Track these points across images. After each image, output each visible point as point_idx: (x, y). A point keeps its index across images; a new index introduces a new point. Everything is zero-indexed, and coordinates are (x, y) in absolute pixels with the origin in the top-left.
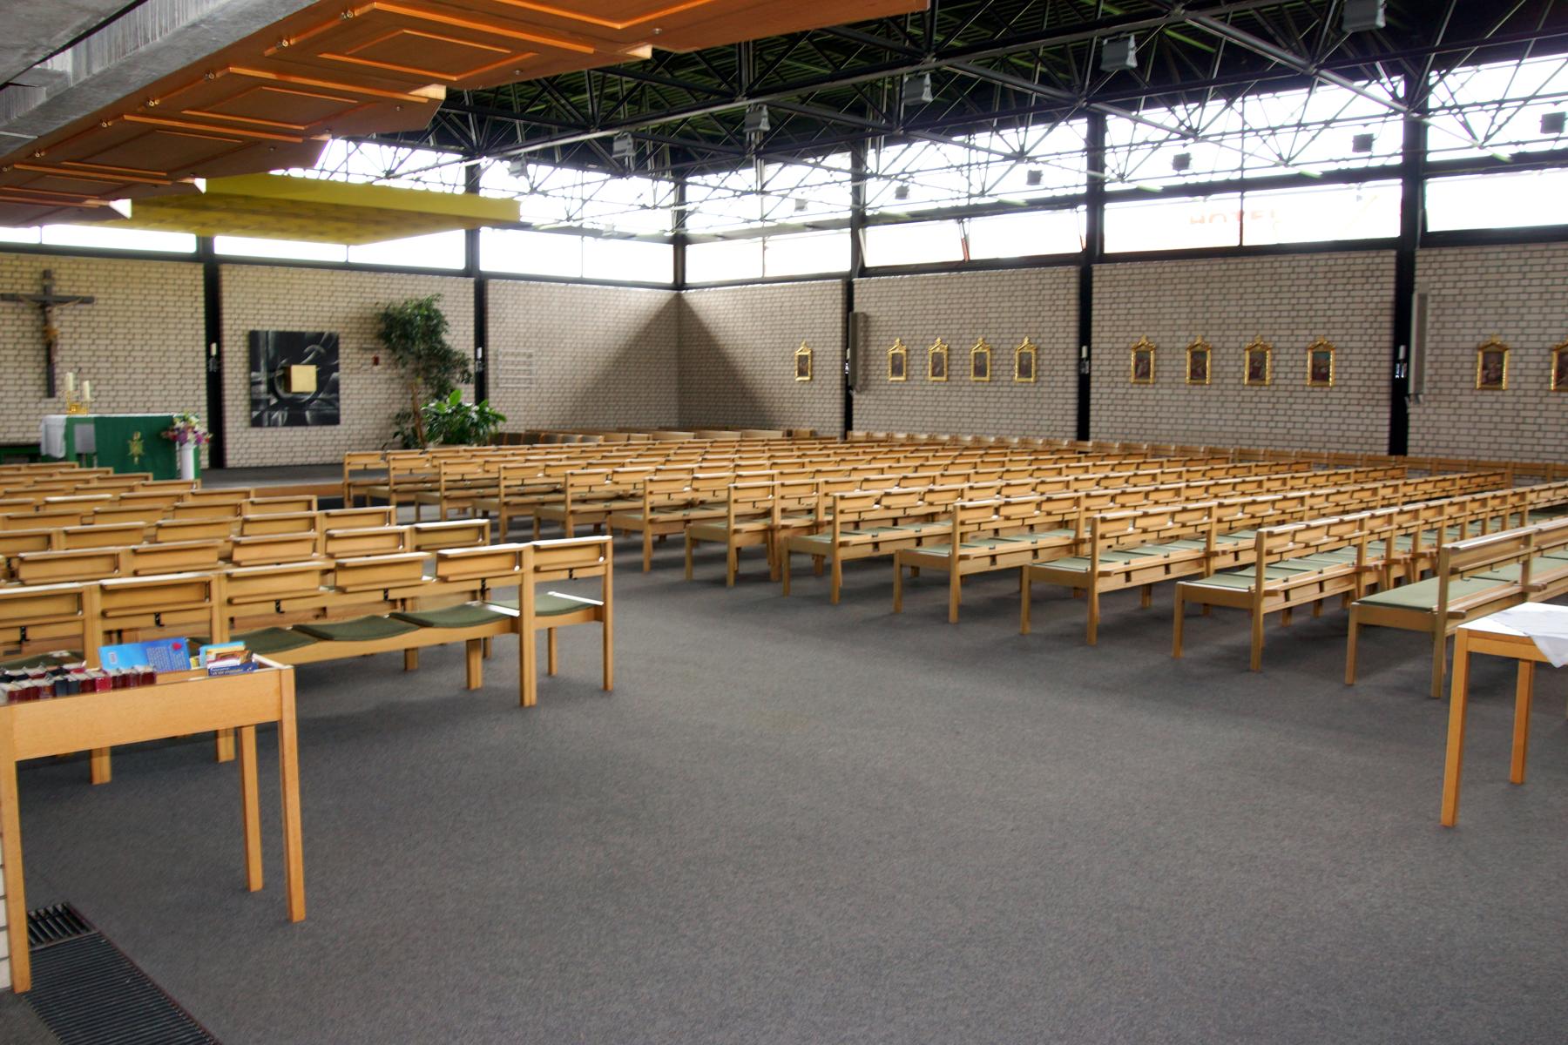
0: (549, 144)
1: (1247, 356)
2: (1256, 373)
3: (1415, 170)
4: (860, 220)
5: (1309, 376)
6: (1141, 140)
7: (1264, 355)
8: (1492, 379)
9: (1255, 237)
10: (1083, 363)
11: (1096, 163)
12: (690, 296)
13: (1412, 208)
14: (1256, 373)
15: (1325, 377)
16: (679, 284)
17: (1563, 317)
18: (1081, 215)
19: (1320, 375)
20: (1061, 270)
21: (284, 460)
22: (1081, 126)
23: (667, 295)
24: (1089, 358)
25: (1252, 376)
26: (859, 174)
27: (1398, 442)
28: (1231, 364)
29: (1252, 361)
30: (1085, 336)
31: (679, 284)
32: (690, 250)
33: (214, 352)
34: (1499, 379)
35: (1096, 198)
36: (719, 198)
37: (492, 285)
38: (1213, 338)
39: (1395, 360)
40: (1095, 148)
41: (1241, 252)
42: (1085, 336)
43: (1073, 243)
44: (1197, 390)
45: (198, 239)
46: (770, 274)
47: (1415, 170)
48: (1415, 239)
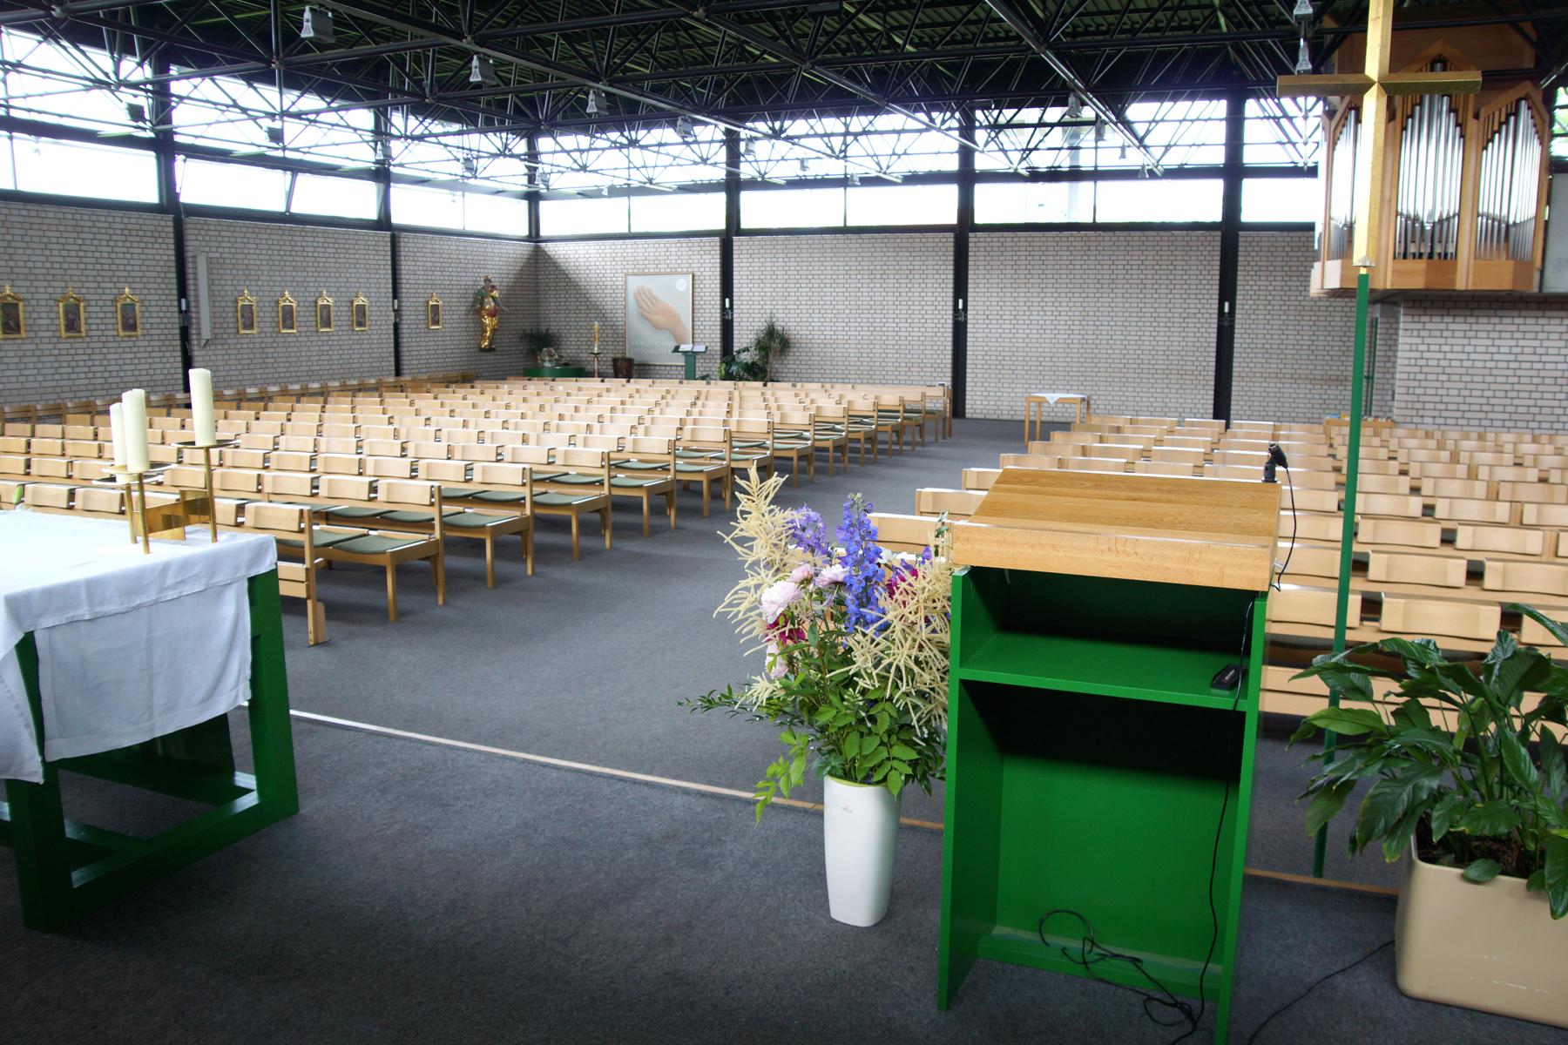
0: (636, 97)
2: (72, 325)
3: (1233, 172)
7: (78, 307)
11: (734, 158)
12: (550, 248)
13: (1232, 202)
14: (72, 325)
16: (534, 236)
17: (1562, 344)
18: (1217, 186)
19: (130, 326)
21: (33, 729)
22: (1220, 107)
23: (527, 247)
26: (967, 130)
29: (67, 313)
31: (534, 236)
35: (733, 186)
36: (790, 147)
37: (190, 222)
40: (1235, 122)
43: (1213, 212)
45: (1363, 71)
48: (1230, 231)
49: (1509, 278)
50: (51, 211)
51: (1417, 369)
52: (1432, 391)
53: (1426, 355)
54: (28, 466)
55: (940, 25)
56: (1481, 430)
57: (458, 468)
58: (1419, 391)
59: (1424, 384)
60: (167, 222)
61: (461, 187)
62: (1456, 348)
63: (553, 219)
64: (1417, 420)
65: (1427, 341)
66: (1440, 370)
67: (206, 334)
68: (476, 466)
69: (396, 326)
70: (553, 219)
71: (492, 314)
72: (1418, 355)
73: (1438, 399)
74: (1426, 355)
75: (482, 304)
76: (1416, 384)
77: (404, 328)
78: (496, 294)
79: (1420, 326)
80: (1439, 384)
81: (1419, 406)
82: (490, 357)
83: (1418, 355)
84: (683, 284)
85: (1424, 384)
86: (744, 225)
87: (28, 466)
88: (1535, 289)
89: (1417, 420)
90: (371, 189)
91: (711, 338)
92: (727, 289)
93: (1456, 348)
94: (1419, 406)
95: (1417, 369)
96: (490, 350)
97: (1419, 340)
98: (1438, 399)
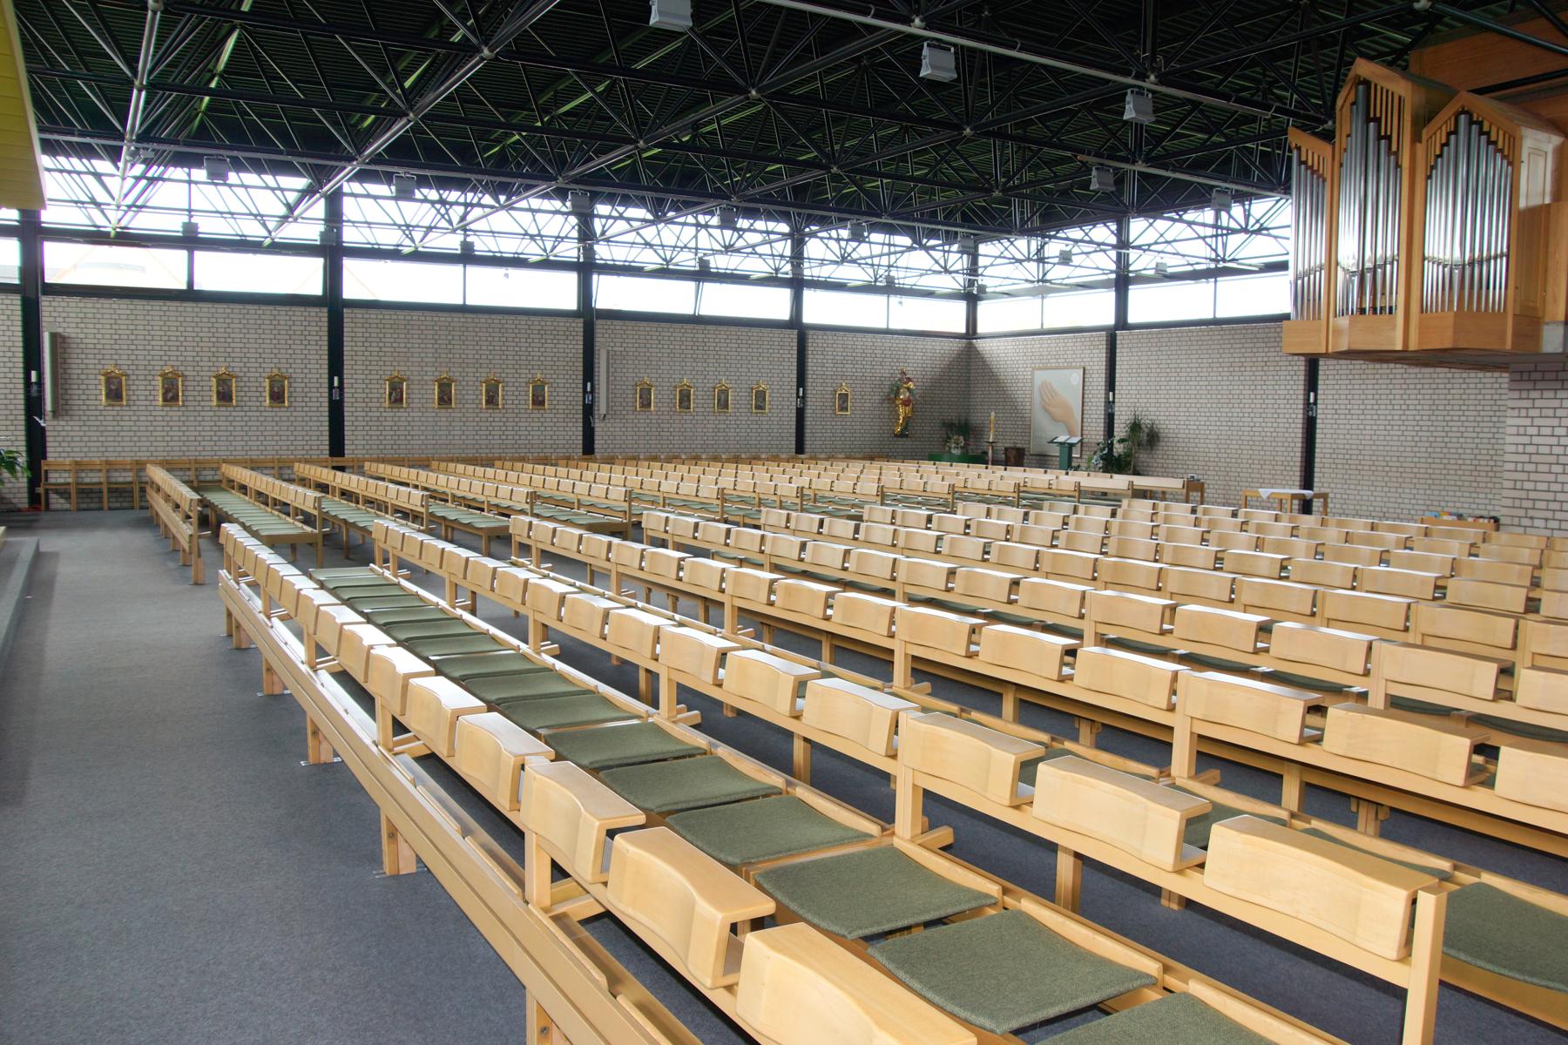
1: (160, 383)
2: (491, 400)
4: (797, 284)
5: (267, 394)
6: (626, 230)
8: (646, 404)
9: (706, 310)
10: (1309, 407)
12: (979, 344)
13: (333, 277)
15: (542, 403)
16: (972, 332)
18: (1110, 296)
19: (538, 401)
20: (313, 310)
23: (957, 345)
24: (1315, 403)
25: (488, 402)
27: (588, 448)
28: (470, 393)
29: (487, 391)
30: (336, 365)
32: (982, 307)
33: (34, 378)
34: (401, 400)
36: (1004, 259)
37: (600, 325)
38: (456, 373)
39: (585, 391)
41: (464, 309)
42: (336, 365)
44: (223, 411)
46: (1047, 326)
47: (1122, 282)
49: (1449, 333)
50: (483, 318)
51: (1526, 458)
52: (1544, 486)
53: (1536, 440)
54: (788, 520)
55: (1387, 54)
56: (1548, 533)
57: (1424, 580)
58: (1528, 485)
59: (1533, 477)
60: (579, 325)
61: (885, 289)
62: (1544, 431)
63: (991, 317)
64: (1526, 522)
65: (1537, 422)
66: (1553, 459)
67: (603, 410)
68: (947, 537)
69: (800, 414)
70: (991, 317)
71: (906, 403)
72: (1526, 440)
73: (1550, 496)
74: (1536, 440)
75: (897, 394)
76: (1524, 476)
77: (808, 412)
78: (911, 385)
79: (1528, 404)
80: (1552, 478)
81: (1528, 504)
82: (901, 441)
83: (1526, 440)
84: (1076, 377)
85: (1533, 477)
86: (1131, 319)
87: (788, 520)
88: (1399, 347)
89: (1526, 522)
90: (785, 294)
91: (1096, 433)
92: (1111, 385)
93: (1544, 431)
94: (1528, 504)
95: (1526, 458)
96: (902, 435)
97: (1528, 422)
98: (1550, 496)
